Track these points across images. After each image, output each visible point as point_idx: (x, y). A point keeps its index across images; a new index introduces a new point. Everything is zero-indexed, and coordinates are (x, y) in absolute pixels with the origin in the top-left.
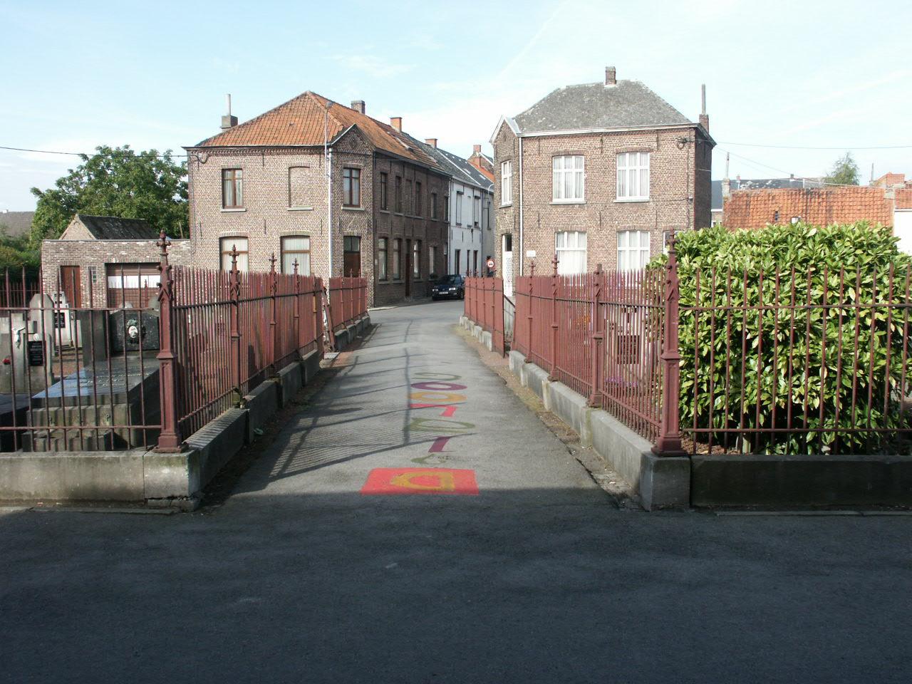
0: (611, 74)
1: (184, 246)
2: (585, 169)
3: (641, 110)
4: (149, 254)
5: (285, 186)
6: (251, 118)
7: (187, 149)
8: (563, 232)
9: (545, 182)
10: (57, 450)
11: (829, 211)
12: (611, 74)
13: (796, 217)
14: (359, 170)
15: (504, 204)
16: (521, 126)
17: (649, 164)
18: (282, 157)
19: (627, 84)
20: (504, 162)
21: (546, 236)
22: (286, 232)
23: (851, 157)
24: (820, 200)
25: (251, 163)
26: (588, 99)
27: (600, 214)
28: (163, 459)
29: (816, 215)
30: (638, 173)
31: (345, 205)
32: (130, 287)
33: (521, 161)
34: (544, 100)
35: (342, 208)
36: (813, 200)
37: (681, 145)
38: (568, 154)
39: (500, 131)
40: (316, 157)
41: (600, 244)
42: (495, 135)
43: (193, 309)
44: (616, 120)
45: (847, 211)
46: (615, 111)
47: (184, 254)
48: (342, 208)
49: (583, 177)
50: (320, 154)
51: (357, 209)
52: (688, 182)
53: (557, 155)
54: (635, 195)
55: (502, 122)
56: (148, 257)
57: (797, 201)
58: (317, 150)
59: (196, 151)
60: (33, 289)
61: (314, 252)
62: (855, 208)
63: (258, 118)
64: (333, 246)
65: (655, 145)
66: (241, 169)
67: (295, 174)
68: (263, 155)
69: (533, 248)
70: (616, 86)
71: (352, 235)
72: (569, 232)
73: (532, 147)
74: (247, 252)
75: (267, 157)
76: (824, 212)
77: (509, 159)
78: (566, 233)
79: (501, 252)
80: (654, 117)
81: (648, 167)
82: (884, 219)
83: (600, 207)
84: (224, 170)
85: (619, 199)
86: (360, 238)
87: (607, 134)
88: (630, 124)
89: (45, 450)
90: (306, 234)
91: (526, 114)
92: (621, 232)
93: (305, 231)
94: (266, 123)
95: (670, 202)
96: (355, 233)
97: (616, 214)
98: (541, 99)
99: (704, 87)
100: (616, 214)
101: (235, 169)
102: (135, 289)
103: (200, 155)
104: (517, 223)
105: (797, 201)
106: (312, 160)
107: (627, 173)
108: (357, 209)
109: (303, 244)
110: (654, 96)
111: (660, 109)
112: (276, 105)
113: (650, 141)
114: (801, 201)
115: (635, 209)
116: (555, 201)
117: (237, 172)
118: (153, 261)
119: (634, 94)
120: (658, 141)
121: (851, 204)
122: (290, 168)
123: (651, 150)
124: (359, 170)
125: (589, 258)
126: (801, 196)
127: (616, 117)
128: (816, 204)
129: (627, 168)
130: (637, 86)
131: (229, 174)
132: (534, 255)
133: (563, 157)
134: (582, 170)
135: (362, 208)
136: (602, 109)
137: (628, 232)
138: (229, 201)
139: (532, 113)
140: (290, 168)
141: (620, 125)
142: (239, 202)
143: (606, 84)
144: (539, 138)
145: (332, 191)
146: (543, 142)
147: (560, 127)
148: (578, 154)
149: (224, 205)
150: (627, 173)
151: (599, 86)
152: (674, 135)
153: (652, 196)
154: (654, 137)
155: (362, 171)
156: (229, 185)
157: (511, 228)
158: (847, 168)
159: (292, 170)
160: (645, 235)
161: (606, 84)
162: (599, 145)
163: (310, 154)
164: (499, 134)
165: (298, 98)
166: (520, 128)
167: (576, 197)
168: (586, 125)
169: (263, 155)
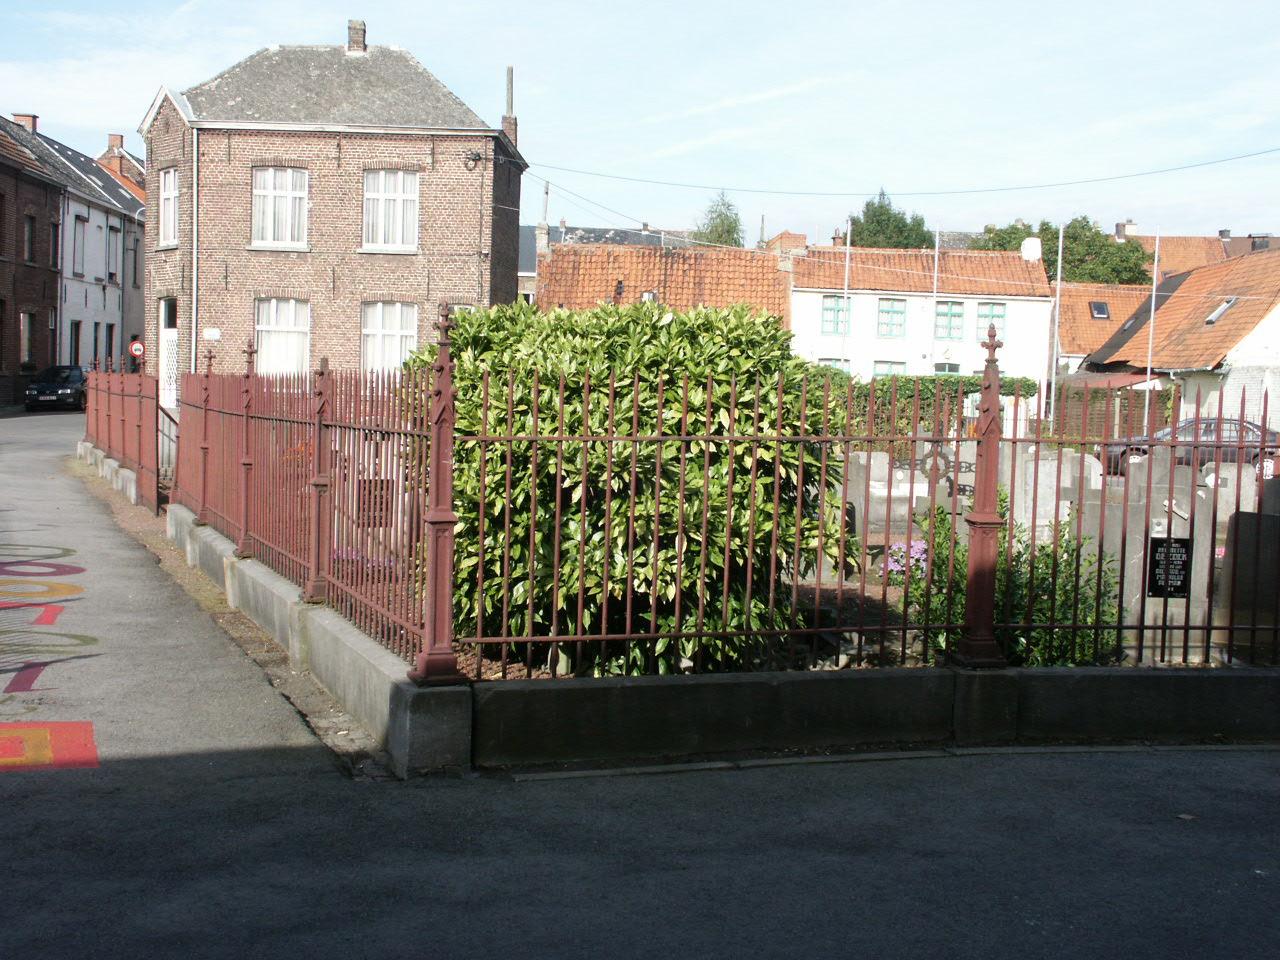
0: (358, 35)
2: (310, 192)
8: (268, 300)
9: (238, 210)
11: (699, 284)
12: (358, 35)
13: (650, 292)
15: (163, 244)
16: (197, 108)
19: (385, 53)
20: (166, 169)
24: (686, 267)
26: (318, 72)
29: (680, 291)
34: (239, 65)
36: (675, 266)
37: (471, 164)
38: (279, 166)
39: (159, 113)
42: (150, 120)
44: (364, 113)
49: (306, 205)
52: (481, 225)
53: (261, 165)
57: (651, 266)
65: (429, 160)
69: (215, 325)
70: (367, 55)
72: (280, 299)
73: (215, 147)
76: (691, 285)
78: (274, 301)
80: (428, 114)
81: (416, 196)
82: (777, 301)
83: (333, 259)
85: (367, 247)
91: (207, 87)
92: (367, 303)
95: (452, 257)
97: (361, 272)
98: (237, 62)
99: (510, 71)
100: (361, 272)
104: (186, 278)
105: (651, 266)
107: (381, 205)
111: (438, 100)
113: (420, 153)
114: (657, 266)
115: (393, 265)
116: (257, 244)
121: (731, 276)
123: (422, 169)
125: (313, 345)
127: (365, 108)
128: (680, 273)
129: (382, 196)
130: (401, 59)
132: (218, 337)
133: (271, 170)
134: (305, 194)
137: (292, 302)
139: (217, 87)
141: (370, 121)
143: (349, 50)
144: (229, 133)
146: (236, 140)
147: (268, 116)
148: (297, 167)
150: (381, 205)
151: (336, 52)
152: (460, 147)
153: (422, 246)
154: (427, 147)
161: (349, 50)
164: (155, 119)
166: (195, 110)
167: (293, 239)
168: (312, 117)
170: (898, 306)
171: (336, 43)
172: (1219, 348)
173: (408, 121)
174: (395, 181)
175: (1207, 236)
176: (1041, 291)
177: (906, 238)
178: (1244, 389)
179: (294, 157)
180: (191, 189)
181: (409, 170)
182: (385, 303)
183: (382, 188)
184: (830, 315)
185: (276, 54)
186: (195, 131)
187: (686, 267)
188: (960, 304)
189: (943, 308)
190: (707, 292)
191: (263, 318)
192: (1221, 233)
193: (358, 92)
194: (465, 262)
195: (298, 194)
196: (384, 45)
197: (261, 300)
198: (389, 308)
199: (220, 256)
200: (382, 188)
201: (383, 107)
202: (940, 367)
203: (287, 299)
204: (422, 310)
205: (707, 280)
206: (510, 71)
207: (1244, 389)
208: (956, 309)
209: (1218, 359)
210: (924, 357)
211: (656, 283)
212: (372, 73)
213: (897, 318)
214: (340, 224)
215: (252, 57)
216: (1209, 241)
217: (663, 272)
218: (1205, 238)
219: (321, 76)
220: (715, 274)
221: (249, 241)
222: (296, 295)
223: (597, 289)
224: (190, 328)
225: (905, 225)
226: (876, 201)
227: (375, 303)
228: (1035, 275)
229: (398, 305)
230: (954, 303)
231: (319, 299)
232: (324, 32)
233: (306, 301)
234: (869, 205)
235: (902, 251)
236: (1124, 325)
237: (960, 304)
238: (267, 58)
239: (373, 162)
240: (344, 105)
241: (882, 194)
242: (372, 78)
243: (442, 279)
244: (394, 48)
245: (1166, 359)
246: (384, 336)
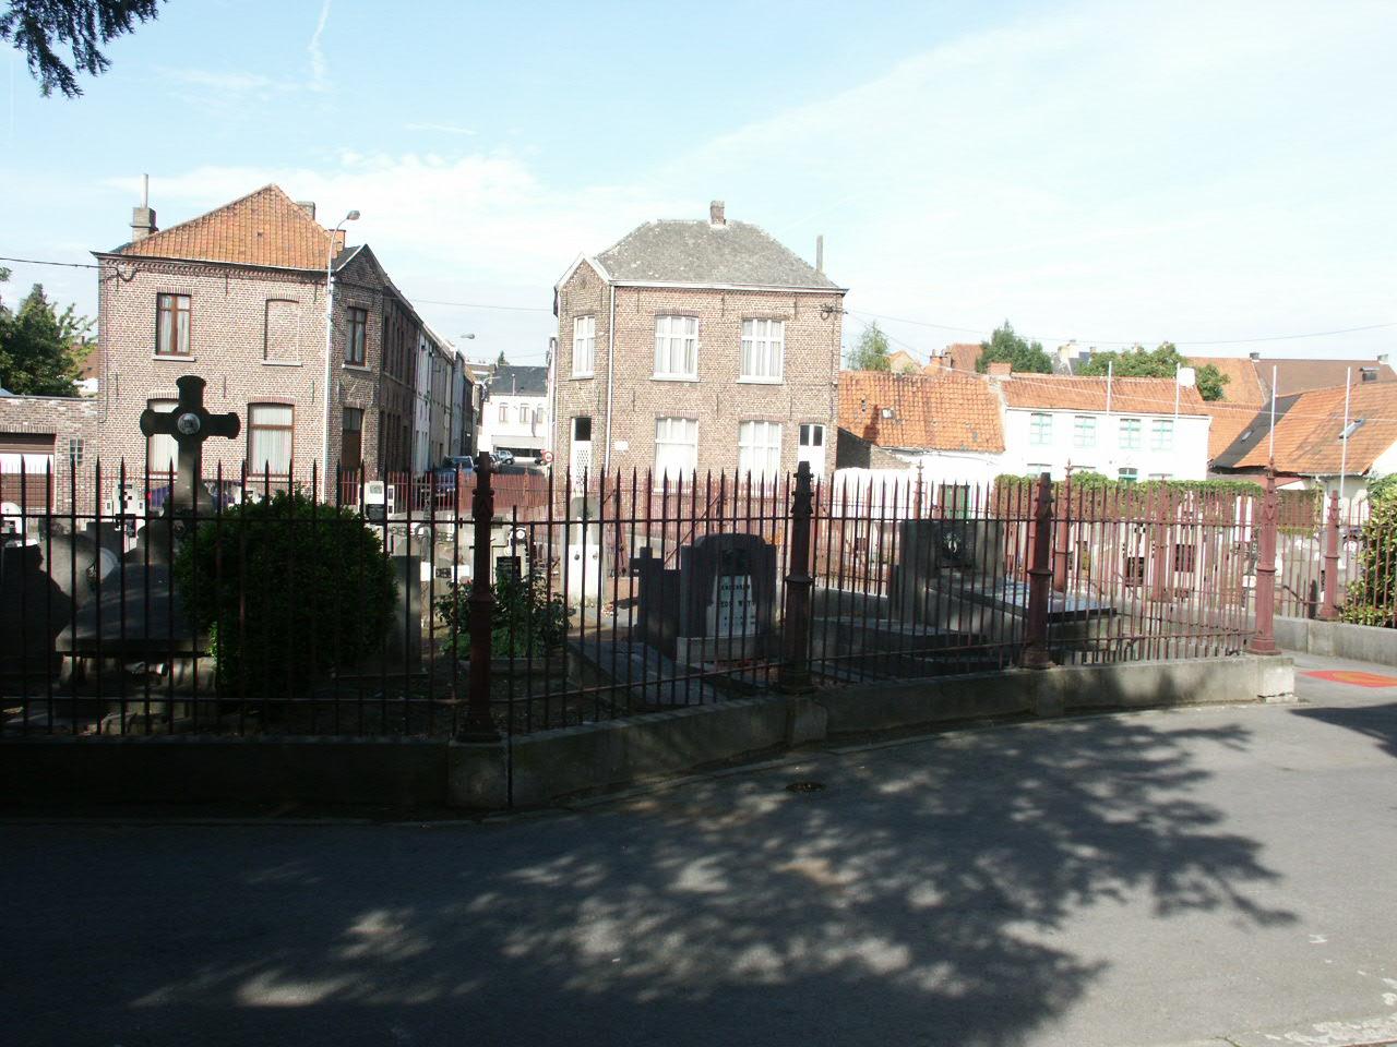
0: (717, 211)
1: (87, 411)
2: (700, 335)
3: (768, 263)
4: (27, 419)
5: (260, 327)
6: (195, 217)
7: (100, 256)
8: (665, 419)
9: (644, 349)
10: (1148, 659)
11: (927, 403)
12: (717, 211)
13: (888, 409)
14: (365, 311)
15: (576, 375)
16: (609, 269)
17: (783, 335)
18: (257, 283)
19: (740, 226)
20: (580, 318)
21: (643, 422)
22: (258, 397)
23: (878, 328)
24: (915, 389)
25: (207, 288)
26: (693, 241)
27: (718, 397)
28: (1278, 661)
29: (912, 408)
30: (768, 345)
31: (346, 362)
32: (9, 472)
33: (612, 318)
34: (631, 235)
35: (343, 366)
36: (906, 389)
37: (825, 315)
38: (676, 315)
39: (575, 273)
40: (309, 288)
41: (717, 436)
42: (568, 276)
43: (1098, 525)
44: (738, 274)
45: (947, 406)
46: (734, 262)
47: (86, 422)
48: (343, 366)
49: (696, 345)
50: (316, 283)
51: (361, 368)
52: (832, 362)
53: (662, 314)
54: (763, 374)
55: (579, 261)
56: (26, 423)
57: (887, 388)
58: (316, 278)
59: (115, 260)
60: (346, 480)
61: (299, 429)
62: (956, 401)
63: (203, 218)
64: (330, 422)
65: (793, 311)
66: (189, 296)
67: (276, 310)
68: (227, 277)
70: (727, 227)
71: (353, 406)
72: (674, 419)
73: (628, 300)
74: (291, 428)
75: (233, 282)
76: (921, 404)
77: (591, 314)
78: (669, 420)
79: (569, 441)
80: (787, 275)
81: (782, 340)
82: (990, 417)
83: (717, 388)
84: (160, 295)
85: (744, 379)
86: (362, 411)
87: (730, 292)
88: (760, 281)
89: (1196, 656)
90: (288, 403)
91: (610, 253)
92: (742, 423)
93: (287, 397)
94: (216, 224)
96: (358, 403)
97: (738, 399)
98: (628, 233)
99: (820, 240)
100: (738, 399)
101: (176, 295)
102: (41, 476)
103: (122, 268)
104: (603, 404)
105: (887, 388)
106: (305, 291)
108: (361, 368)
109: (284, 416)
110: (780, 247)
111: (792, 265)
112: (228, 201)
113: (786, 306)
114: (891, 388)
115: (763, 393)
116: (657, 376)
117: (180, 300)
118: (34, 431)
119: (745, 240)
120: (795, 307)
121: (951, 396)
122: (268, 301)
123: (786, 318)
124: (365, 311)
125: (700, 455)
126: (891, 383)
127: (737, 270)
128: (910, 394)
129: (754, 338)
130: (752, 231)
131: (167, 302)
133: (670, 318)
134: (695, 336)
135: (367, 368)
136: (715, 258)
137: (752, 423)
138: (166, 345)
139: (619, 253)
140: (268, 301)
141: (745, 281)
142: (183, 346)
143: (713, 223)
144: (639, 289)
145: (333, 340)
146: (643, 295)
147: (666, 276)
148: (691, 316)
149: (158, 351)
151: (702, 225)
152: (817, 302)
153: (786, 378)
154: (791, 302)
155: (370, 314)
156: (167, 318)
157: (590, 409)
158: (876, 342)
159: (271, 303)
160: (775, 427)
161: (713, 223)
162: (718, 305)
163: (301, 283)
164: (572, 278)
165: (259, 193)
166: (608, 272)
167: (758, 374)
168: (700, 277)
169: (227, 277)
170: (1089, 422)
171: (701, 218)
172: (1364, 458)
173: (774, 281)
174: (765, 328)
175: (1241, 357)
176: (1200, 411)
177: (1029, 361)
178: (315, 465)
179: (688, 308)
180: (606, 333)
181: (776, 319)
182: (756, 422)
183: (769, 333)
184: (1036, 428)
185: (657, 226)
186: (613, 288)
187: (915, 389)
188: (1138, 420)
189: (1126, 424)
190: (933, 410)
191: (661, 433)
192: (1252, 355)
193: (728, 257)
194: (819, 390)
195: (690, 337)
196: (739, 220)
197: (659, 419)
198: (759, 426)
199: (629, 385)
200: (769, 333)
201: (752, 270)
202: (1122, 471)
203: (680, 419)
204: (786, 428)
205: (933, 400)
206: (820, 240)
207: (315, 465)
208: (1135, 425)
209: (1366, 468)
210: (1111, 462)
211: (892, 403)
212: (736, 243)
213: (1089, 432)
214: (723, 361)
215: (639, 229)
216: (1242, 362)
217: (897, 393)
218: (1239, 360)
219: (696, 245)
220: (938, 395)
221: (652, 374)
222: (688, 416)
223: (846, 406)
224: (605, 441)
225: (1027, 350)
226: (1002, 329)
227: (748, 422)
228: (1193, 398)
229: (767, 423)
230: (1133, 420)
231: (707, 419)
232: (694, 211)
233: (694, 421)
234: (996, 333)
235: (1085, 378)
236: (1240, 436)
237: (1138, 420)
238: (651, 229)
239: (749, 312)
240: (721, 267)
241: (1007, 324)
242: (736, 246)
243: (802, 403)
244: (745, 222)
245: (1303, 465)
246: (755, 448)
